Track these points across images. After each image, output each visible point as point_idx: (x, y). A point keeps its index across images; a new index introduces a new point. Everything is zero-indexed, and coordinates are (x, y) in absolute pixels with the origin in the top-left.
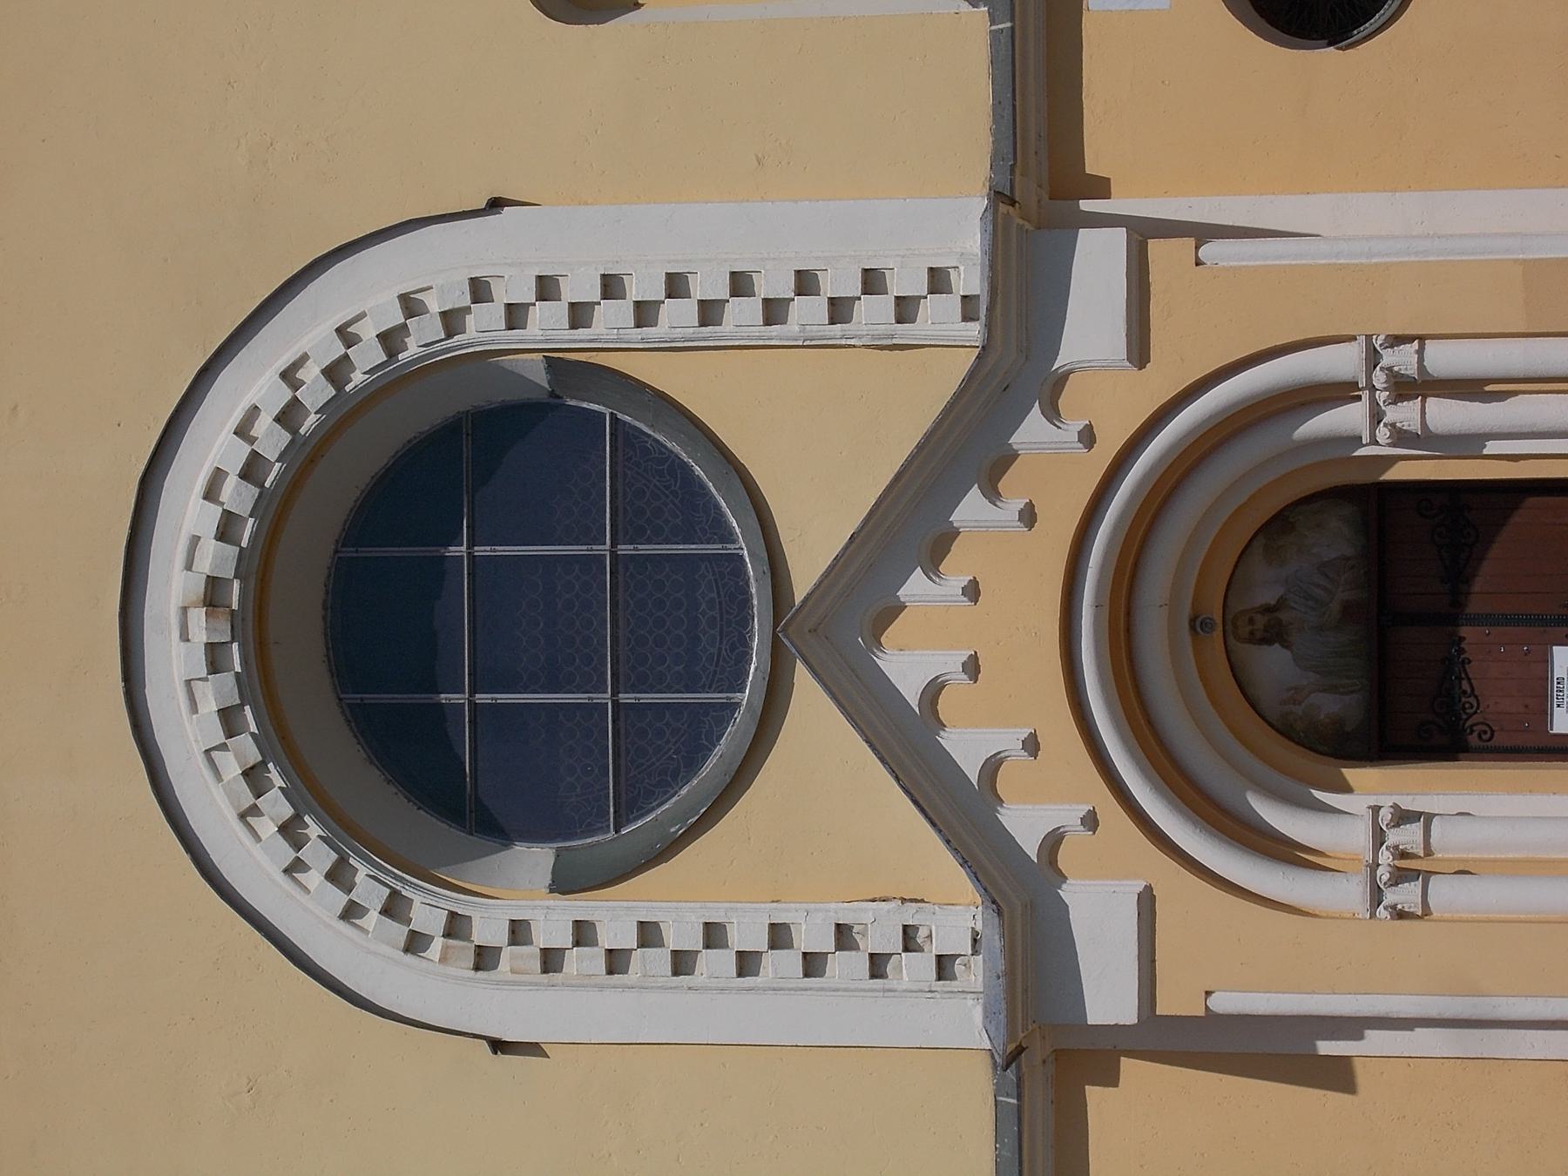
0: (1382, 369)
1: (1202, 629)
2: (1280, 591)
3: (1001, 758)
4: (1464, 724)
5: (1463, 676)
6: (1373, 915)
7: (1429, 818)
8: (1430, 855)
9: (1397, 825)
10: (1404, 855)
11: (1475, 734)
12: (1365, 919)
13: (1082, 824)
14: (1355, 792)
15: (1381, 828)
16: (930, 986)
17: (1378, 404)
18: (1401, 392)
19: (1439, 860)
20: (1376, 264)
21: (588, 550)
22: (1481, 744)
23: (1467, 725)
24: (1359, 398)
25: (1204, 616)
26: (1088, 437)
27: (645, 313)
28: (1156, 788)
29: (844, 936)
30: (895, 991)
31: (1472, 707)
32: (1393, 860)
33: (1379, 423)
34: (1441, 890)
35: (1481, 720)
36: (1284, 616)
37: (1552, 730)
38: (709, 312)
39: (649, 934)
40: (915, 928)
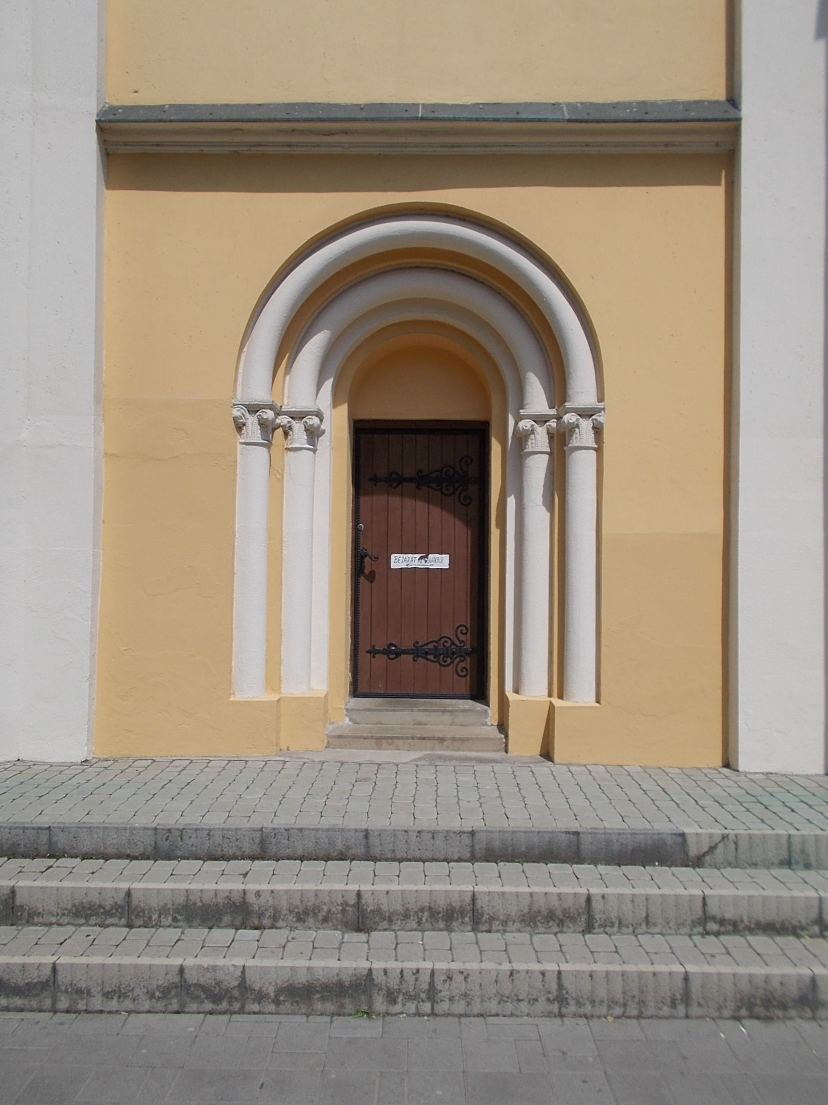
7: (314, 451)
9: (306, 430)
14: (333, 411)
15: (304, 418)
18: (555, 437)
24: (551, 407)
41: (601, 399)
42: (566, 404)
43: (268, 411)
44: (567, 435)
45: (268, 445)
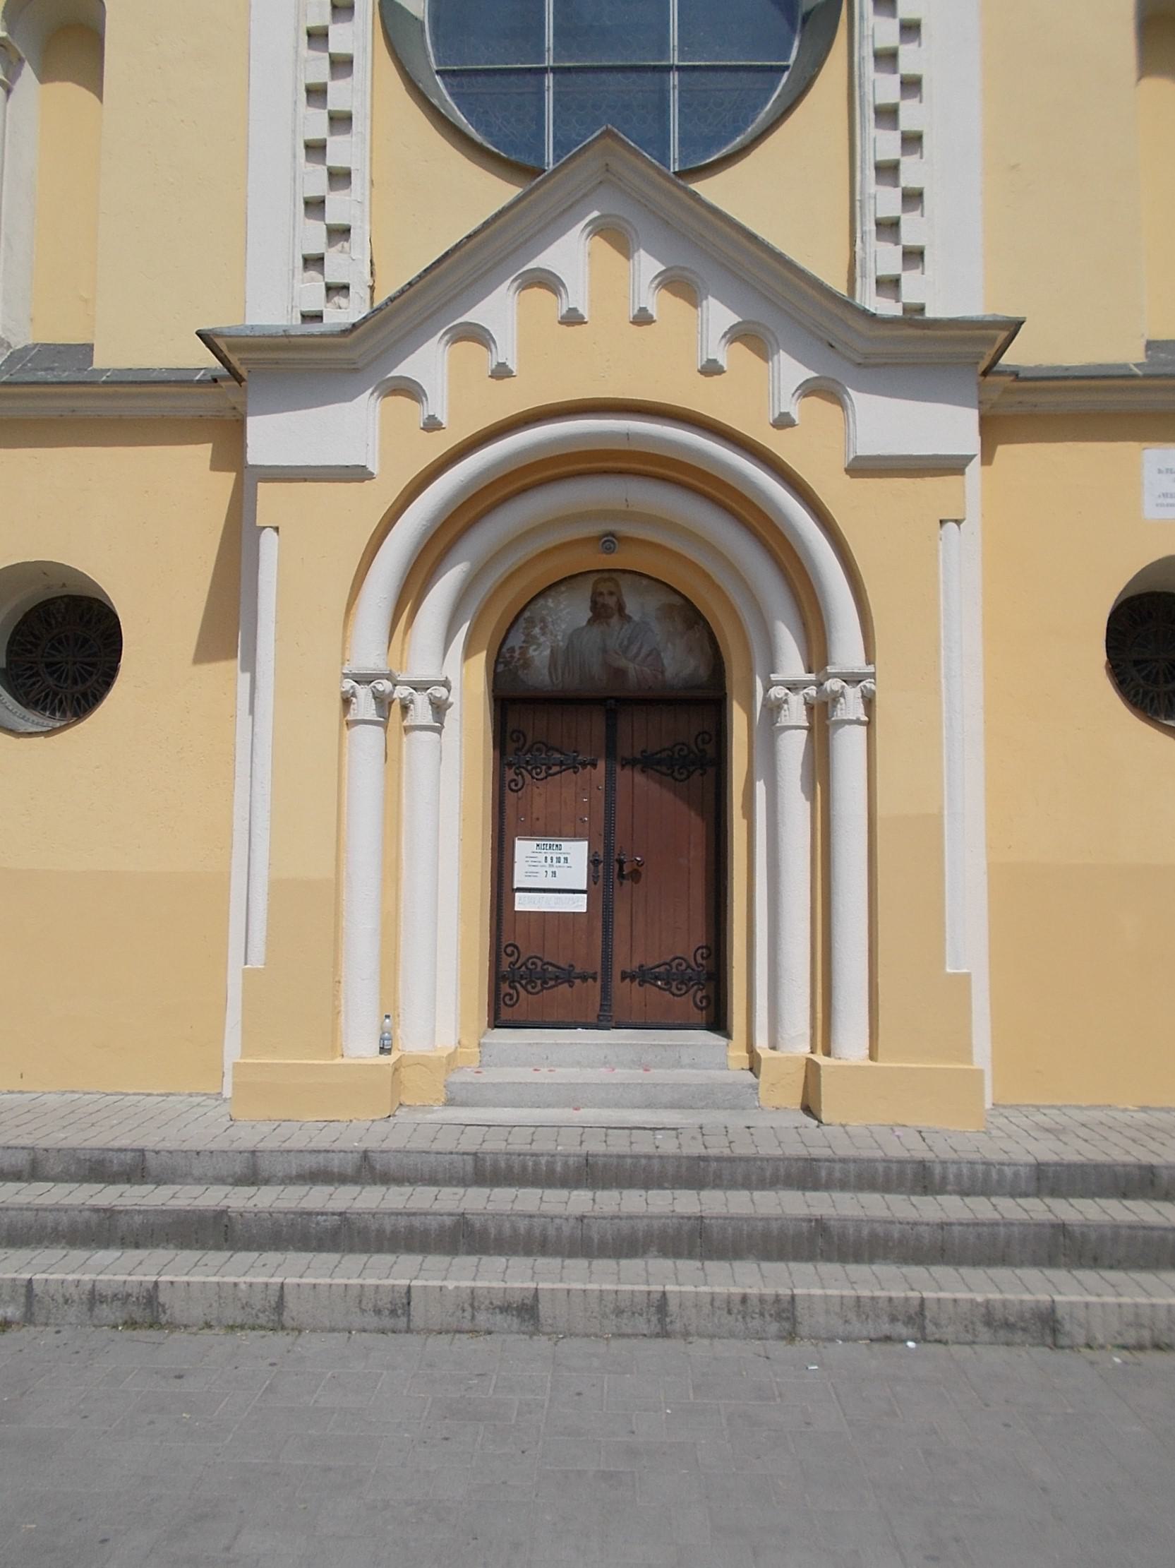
0: (843, 687)
1: (606, 541)
2: (636, 618)
3: (489, 345)
4: (523, 768)
5: (564, 767)
6: (346, 676)
7: (439, 730)
8: (405, 731)
9: (432, 703)
10: (405, 709)
11: (515, 777)
12: (342, 669)
13: (429, 416)
15: (428, 688)
16: (296, 307)
17: (805, 688)
18: (815, 707)
19: (401, 739)
20: (940, 681)
21: (674, 46)
22: (507, 783)
23: (523, 770)
25: (617, 546)
26: (784, 422)
27: (887, 58)
28: (464, 488)
29: (340, 233)
30: (293, 278)
31: (537, 774)
32: (400, 699)
33: (789, 689)
34: (368, 740)
35: (527, 782)
36: (615, 620)
37: (519, 839)
38: (887, 115)
39: (341, 65)
40: (347, 296)
41: (870, 660)
42: (828, 667)
43: (385, 681)
44: (830, 705)
45: (384, 725)
